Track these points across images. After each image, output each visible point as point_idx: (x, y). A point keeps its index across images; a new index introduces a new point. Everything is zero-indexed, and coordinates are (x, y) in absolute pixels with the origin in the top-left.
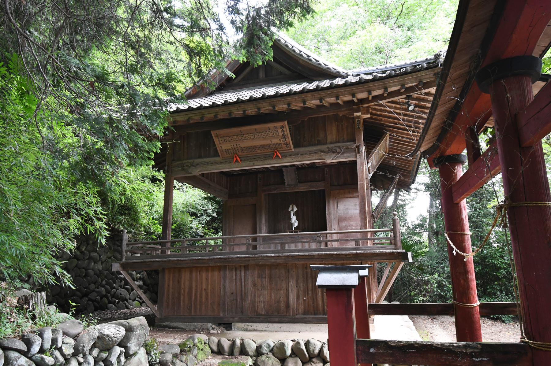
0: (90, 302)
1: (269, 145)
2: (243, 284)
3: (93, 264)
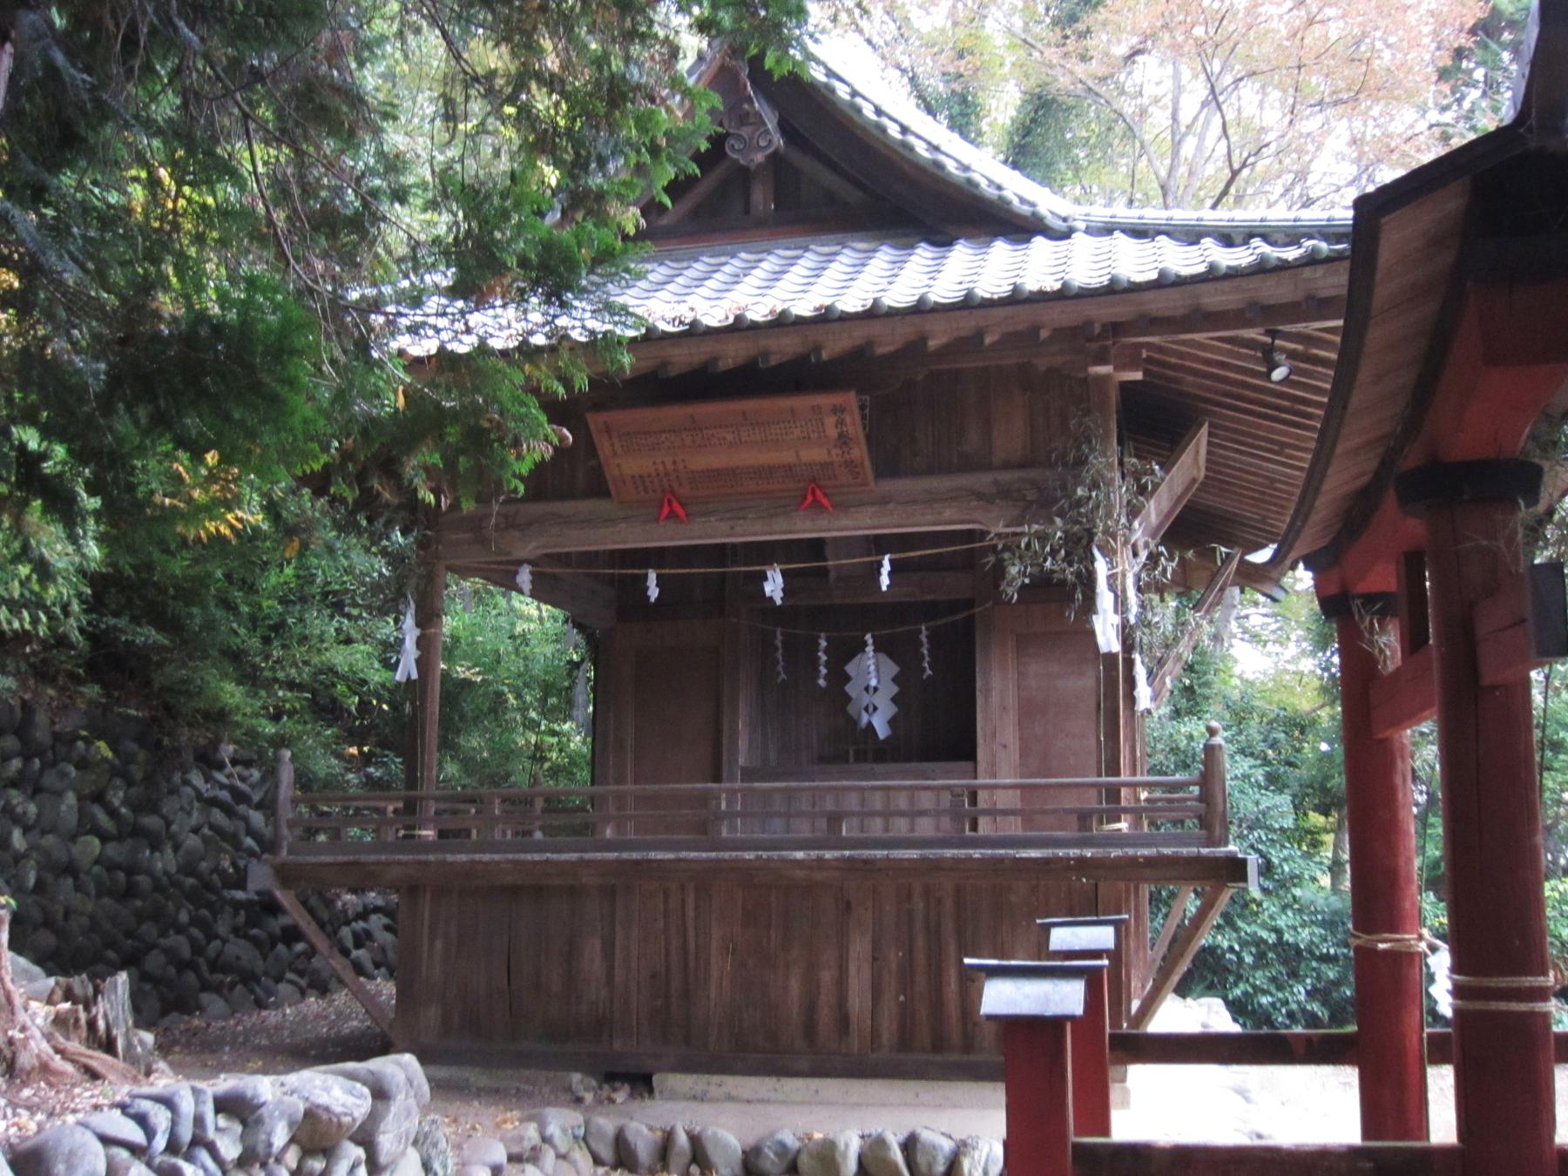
0: (148, 987)
1: (789, 469)
2: (692, 945)
3: (148, 853)
